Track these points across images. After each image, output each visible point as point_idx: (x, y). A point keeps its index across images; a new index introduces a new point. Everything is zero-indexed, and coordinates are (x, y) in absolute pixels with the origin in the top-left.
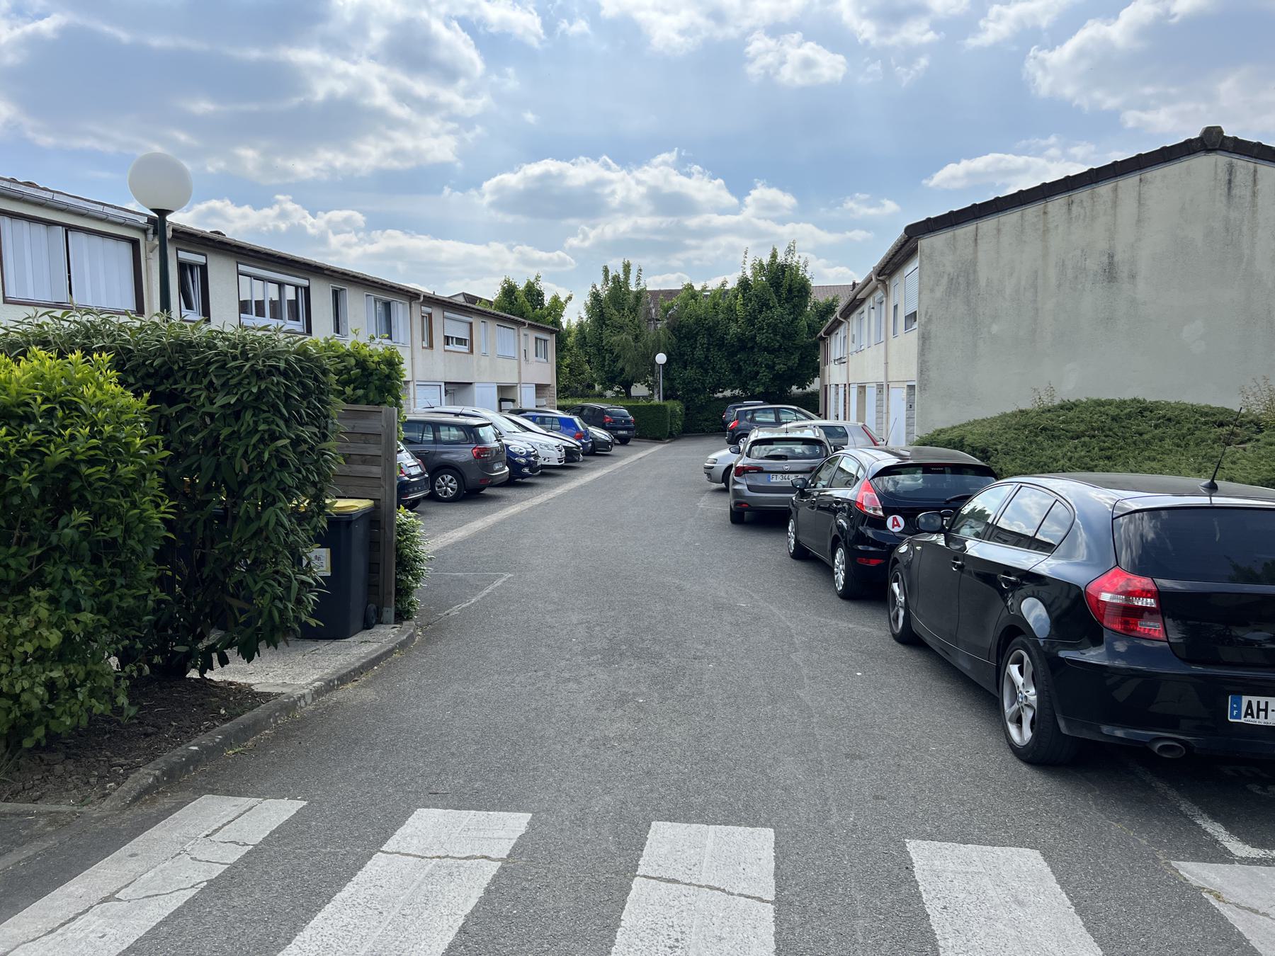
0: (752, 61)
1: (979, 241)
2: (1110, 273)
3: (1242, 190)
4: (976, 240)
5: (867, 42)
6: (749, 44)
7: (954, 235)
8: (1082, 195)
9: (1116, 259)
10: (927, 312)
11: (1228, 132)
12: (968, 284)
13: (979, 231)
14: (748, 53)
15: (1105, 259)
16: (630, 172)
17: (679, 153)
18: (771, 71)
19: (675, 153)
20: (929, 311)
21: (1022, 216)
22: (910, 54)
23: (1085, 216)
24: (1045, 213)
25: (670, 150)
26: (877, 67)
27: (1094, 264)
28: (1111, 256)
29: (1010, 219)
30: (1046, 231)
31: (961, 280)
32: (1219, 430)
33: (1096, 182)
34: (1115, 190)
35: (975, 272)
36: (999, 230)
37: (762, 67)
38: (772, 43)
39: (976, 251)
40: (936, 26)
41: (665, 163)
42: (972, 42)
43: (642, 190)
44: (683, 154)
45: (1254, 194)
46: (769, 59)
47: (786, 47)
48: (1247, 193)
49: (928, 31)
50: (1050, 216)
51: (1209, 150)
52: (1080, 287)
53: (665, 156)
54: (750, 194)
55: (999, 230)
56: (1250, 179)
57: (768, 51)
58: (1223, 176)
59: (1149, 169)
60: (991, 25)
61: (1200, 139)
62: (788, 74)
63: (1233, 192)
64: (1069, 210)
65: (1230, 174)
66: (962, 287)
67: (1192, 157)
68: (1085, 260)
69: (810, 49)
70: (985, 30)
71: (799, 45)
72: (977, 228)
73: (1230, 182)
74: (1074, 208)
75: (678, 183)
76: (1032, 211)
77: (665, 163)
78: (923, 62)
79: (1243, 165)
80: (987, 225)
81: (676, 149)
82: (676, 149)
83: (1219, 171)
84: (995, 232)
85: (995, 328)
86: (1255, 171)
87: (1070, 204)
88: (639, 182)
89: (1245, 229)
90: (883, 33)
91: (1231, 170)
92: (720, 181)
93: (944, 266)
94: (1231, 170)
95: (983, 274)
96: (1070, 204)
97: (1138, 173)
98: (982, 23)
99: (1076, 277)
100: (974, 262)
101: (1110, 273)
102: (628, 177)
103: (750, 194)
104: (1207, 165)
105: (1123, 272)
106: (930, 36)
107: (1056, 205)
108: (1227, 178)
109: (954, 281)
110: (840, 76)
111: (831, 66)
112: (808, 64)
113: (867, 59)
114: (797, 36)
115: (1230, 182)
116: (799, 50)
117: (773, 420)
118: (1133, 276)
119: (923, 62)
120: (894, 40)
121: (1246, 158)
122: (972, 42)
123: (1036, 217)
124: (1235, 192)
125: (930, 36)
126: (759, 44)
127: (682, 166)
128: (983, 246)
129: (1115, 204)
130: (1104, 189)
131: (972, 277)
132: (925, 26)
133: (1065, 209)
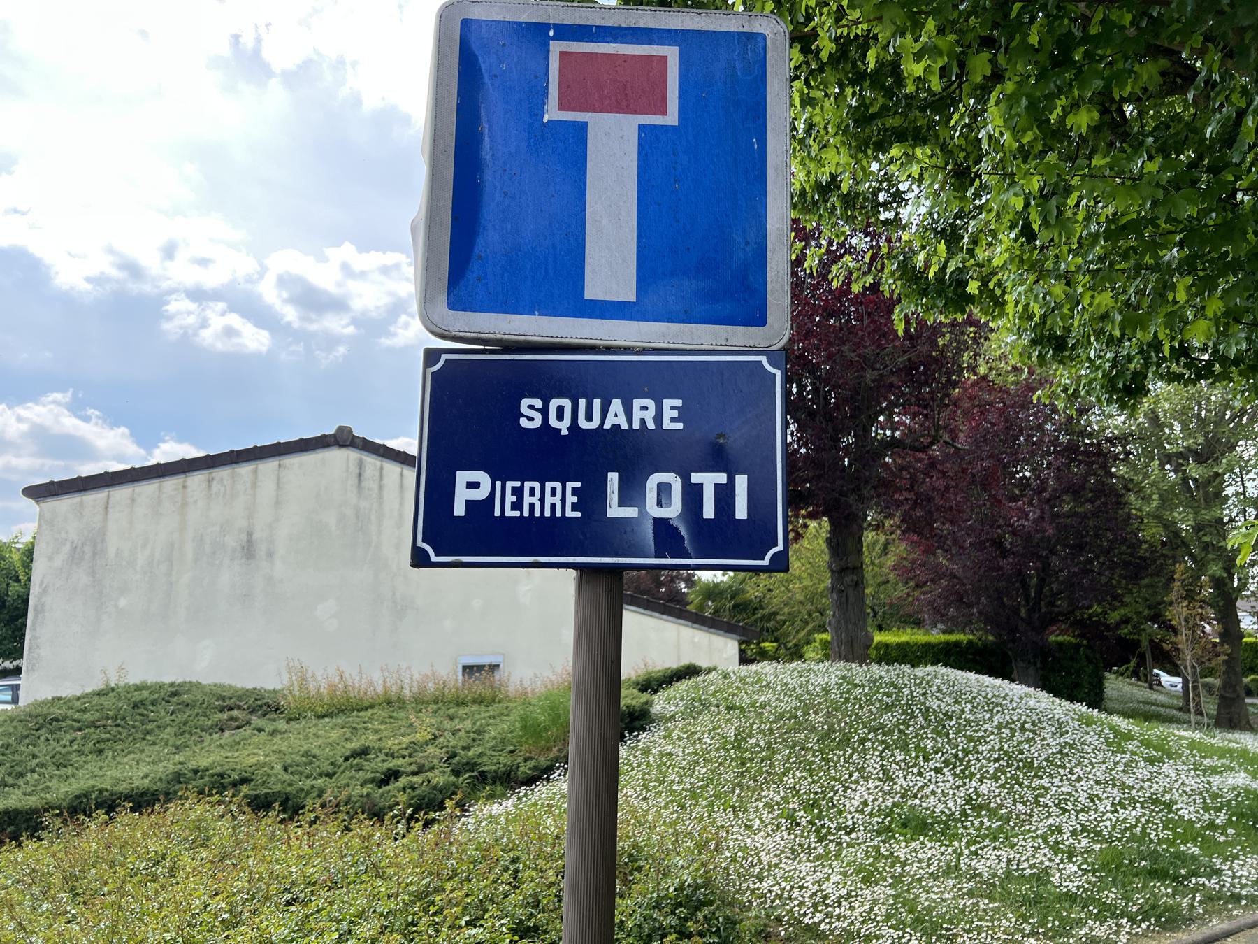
0: (170, 318)
1: (110, 510)
2: (248, 550)
3: (370, 484)
4: (106, 508)
5: (289, 323)
6: (168, 303)
7: (82, 501)
8: (223, 473)
9: (254, 537)
10: (42, 582)
11: (357, 433)
12: (94, 554)
13: (111, 499)
14: (167, 311)
15: (244, 537)
16: (10, 407)
17: (75, 395)
18: (190, 332)
19: (69, 394)
20: (45, 582)
21: (160, 488)
22: (331, 341)
23: (225, 493)
24: (184, 487)
25: (64, 391)
26: (300, 348)
27: (232, 541)
28: (250, 534)
29: (147, 489)
30: (185, 504)
31: (87, 549)
32: (220, 715)
33: (237, 463)
34: (255, 472)
35: (103, 541)
36: (133, 500)
37: (181, 327)
38: (193, 306)
39: (105, 520)
40: (355, 322)
41: (55, 402)
42: (385, 342)
43: (24, 427)
44: (80, 395)
45: (381, 488)
46: (191, 320)
47: (208, 313)
48: (375, 486)
49: (349, 325)
50: (189, 490)
51: (342, 446)
52: (217, 562)
53: (58, 396)
54: (158, 447)
55: (133, 500)
56: (377, 474)
57: (189, 313)
58: (354, 469)
59: (287, 456)
60: (400, 331)
61: (334, 436)
62: (207, 336)
63: (363, 484)
64: (210, 487)
65: (360, 468)
66: (86, 557)
67: (326, 449)
68: (224, 536)
69: (235, 320)
70: (395, 335)
71: (223, 314)
72: (108, 496)
73: (360, 475)
74: (214, 484)
75: (70, 423)
76: (170, 484)
77: (55, 402)
78: (342, 350)
79: (371, 461)
80: (121, 494)
81: (71, 390)
82: (71, 390)
83: (351, 465)
84: (129, 502)
85: (122, 602)
86: (382, 468)
87: (210, 481)
88: (20, 419)
89: (373, 517)
90: (304, 319)
91: (361, 464)
92: (123, 430)
93: (67, 533)
94: (361, 464)
95: (113, 544)
96: (210, 481)
97: (277, 458)
98: (392, 329)
99: (214, 553)
100: (103, 531)
101: (248, 550)
102: (9, 412)
103: (158, 447)
104: (346, 457)
105: (261, 550)
106: (350, 330)
107: (197, 480)
108: (357, 471)
109: (78, 550)
110: (264, 349)
111: (255, 339)
112: (230, 332)
113: (290, 339)
114: (221, 306)
115: (360, 475)
116: (219, 319)
117: (9, 698)
118: (270, 555)
119: (342, 350)
120: (314, 327)
121: (374, 456)
122: (385, 342)
123: (175, 489)
124: (365, 484)
125: (350, 330)
126: (178, 305)
127: (76, 408)
128: (114, 515)
129: (254, 485)
130: (245, 470)
131: (99, 547)
132: (345, 321)
133: (205, 484)
